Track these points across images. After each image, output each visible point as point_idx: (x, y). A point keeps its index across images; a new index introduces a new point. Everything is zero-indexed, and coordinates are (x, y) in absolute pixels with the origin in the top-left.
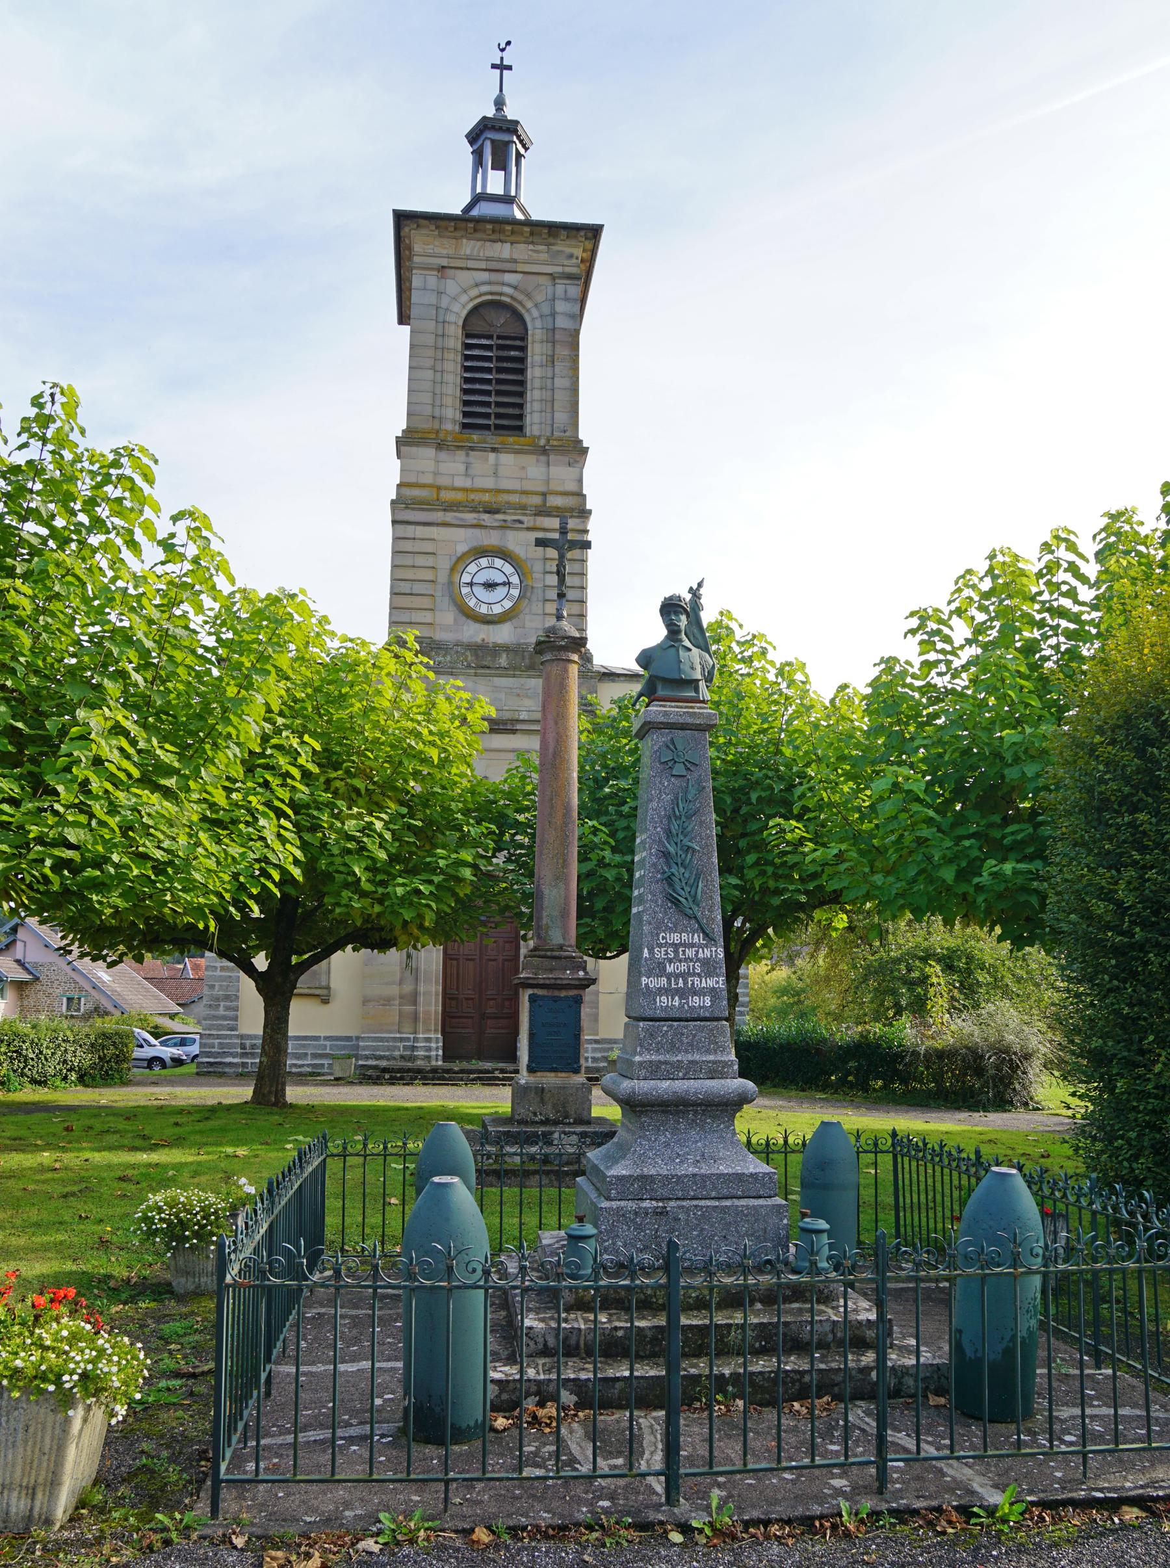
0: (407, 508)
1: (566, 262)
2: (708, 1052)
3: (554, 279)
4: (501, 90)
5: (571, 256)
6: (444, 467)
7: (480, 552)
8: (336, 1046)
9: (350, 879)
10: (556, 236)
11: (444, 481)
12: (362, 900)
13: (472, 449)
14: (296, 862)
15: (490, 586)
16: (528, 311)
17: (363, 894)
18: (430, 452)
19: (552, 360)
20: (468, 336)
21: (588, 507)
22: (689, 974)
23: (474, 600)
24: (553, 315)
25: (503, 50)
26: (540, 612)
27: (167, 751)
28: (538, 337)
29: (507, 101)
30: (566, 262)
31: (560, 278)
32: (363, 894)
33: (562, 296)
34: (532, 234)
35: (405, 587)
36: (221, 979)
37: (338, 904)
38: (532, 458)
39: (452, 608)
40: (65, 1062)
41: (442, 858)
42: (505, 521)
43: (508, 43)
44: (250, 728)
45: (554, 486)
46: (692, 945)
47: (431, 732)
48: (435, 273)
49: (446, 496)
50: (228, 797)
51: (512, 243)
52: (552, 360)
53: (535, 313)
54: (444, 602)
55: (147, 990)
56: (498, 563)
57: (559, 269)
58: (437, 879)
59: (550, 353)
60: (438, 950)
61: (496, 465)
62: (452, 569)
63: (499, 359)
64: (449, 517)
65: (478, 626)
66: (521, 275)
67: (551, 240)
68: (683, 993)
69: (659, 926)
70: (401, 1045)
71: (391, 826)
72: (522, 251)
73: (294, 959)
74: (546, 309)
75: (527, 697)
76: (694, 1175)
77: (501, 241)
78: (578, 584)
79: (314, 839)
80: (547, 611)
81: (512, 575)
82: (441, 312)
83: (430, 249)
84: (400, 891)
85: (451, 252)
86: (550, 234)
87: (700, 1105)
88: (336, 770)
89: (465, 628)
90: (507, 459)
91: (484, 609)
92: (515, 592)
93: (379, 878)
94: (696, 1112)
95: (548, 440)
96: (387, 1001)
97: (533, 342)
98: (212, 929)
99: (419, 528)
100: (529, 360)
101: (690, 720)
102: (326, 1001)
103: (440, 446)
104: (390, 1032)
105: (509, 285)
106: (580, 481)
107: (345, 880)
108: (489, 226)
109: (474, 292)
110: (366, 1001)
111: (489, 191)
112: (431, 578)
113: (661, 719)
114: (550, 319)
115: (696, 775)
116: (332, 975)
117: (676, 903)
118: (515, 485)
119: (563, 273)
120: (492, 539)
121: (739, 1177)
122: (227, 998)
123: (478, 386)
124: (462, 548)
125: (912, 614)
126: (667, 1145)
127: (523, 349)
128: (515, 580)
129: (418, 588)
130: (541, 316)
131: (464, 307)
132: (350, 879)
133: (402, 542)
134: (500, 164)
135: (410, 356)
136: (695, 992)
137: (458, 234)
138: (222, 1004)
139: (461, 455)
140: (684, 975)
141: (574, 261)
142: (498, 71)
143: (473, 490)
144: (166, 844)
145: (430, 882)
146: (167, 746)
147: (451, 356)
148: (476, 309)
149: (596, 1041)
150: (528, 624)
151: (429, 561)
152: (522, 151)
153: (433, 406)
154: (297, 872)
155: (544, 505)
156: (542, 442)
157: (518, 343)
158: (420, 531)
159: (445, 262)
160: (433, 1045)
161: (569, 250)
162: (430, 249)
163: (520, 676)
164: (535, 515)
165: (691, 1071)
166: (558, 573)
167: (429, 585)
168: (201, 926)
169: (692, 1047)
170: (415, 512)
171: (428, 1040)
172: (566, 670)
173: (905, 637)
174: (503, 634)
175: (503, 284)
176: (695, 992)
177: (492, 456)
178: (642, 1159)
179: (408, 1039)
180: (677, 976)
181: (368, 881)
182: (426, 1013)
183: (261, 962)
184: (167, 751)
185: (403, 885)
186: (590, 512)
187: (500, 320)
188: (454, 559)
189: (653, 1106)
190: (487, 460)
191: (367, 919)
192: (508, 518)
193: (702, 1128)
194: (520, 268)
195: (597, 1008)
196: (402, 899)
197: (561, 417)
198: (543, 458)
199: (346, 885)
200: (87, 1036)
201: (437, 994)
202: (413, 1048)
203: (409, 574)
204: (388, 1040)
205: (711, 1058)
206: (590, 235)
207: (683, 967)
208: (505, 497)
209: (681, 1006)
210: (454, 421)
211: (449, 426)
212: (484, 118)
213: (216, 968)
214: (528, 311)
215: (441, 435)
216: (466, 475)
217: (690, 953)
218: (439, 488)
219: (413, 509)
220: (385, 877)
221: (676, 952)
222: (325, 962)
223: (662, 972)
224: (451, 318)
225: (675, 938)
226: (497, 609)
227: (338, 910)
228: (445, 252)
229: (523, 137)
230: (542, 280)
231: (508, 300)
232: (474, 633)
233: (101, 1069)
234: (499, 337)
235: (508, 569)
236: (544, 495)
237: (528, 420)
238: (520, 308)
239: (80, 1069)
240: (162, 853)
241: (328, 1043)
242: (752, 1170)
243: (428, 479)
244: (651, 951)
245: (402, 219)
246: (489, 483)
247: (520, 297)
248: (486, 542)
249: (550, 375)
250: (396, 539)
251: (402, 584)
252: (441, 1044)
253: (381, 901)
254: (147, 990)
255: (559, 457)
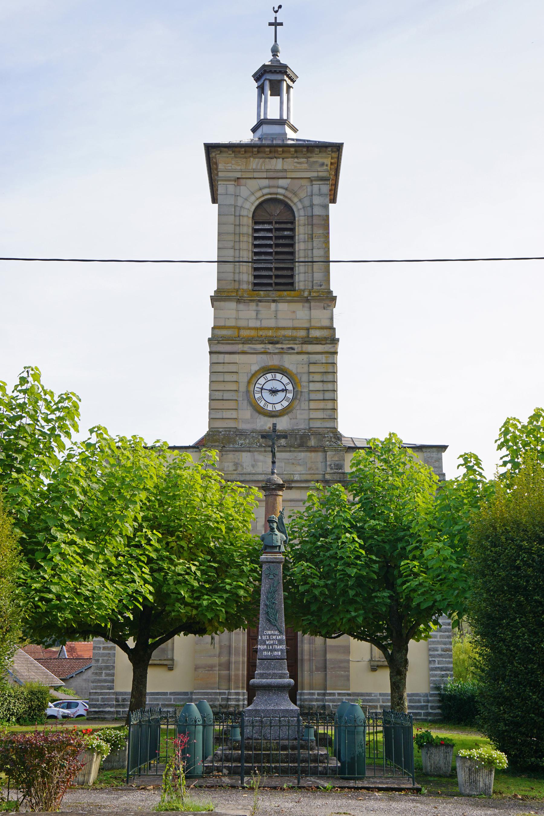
0: (218, 343)
1: (319, 169)
2: (279, 670)
3: (312, 181)
4: (276, 41)
5: (323, 164)
6: (242, 315)
7: (266, 370)
8: (178, 698)
9: (179, 596)
10: (312, 152)
11: (242, 323)
12: (186, 608)
13: (260, 301)
14: (151, 593)
15: (274, 392)
16: (295, 204)
17: (186, 604)
18: (233, 305)
19: (311, 237)
20: (256, 223)
21: (337, 337)
22: (274, 644)
23: (263, 402)
24: (312, 206)
25: (276, 12)
26: (307, 408)
27: (91, 544)
28: (302, 222)
29: (280, 48)
30: (319, 169)
31: (315, 180)
32: (186, 604)
33: (317, 192)
34: (296, 152)
35: (218, 395)
36: (103, 655)
37: (174, 611)
38: (300, 305)
39: (249, 408)
40: (9, 709)
41: (228, 584)
42: (282, 348)
43: (280, 7)
44: (128, 528)
45: (314, 323)
46: (275, 635)
47: (221, 517)
48: (233, 183)
49: (244, 333)
50: (117, 560)
51: (283, 159)
52: (311, 237)
53: (300, 206)
54: (244, 404)
55: (37, 668)
56: (279, 376)
57: (315, 174)
58: (225, 596)
59: (310, 232)
60: (243, 634)
61: (276, 311)
62: (249, 382)
63: (277, 238)
64: (246, 347)
65: (266, 419)
66: (290, 180)
67: (309, 155)
68: (271, 651)
69: (265, 629)
70: (219, 697)
71: (202, 567)
72: (289, 164)
73: (150, 641)
74: (307, 203)
75: (300, 465)
76: (273, 709)
77: (276, 158)
78: (331, 388)
79: (159, 576)
80: (311, 408)
81: (288, 384)
82: (238, 209)
83: (229, 167)
84: (205, 603)
85: (243, 167)
86: (308, 151)
87: (276, 687)
88: (172, 537)
89: (258, 420)
90: (283, 306)
91: (270, 408)
92: (290, 396)
93: (195, 595)
94: (275, 690)
95: (310, 292)
96: (211, 667)
97: (299, 226)
98: (109, 627)
99: (227, 356)
100: (297, 237)
101: (275, 560)
102: (171, 669)
103: (239, 301)
104: (213, 689)
105: (282, 188)
106: (332, 319)
107: (177, 597)
108: (268, 150)
109: (259, 194)
110: (197, 668)
111: (269, 117)
112: (235, 388)
113: (265, 560)
114: (309, 209)
115: (277, 578)
116: (175, 651)
117: (270, 621)
118: (289, 324)
119: (318, 177)
120: (275, 361)
121: (287, 711)
122: (107, 668)
123: (263, 257)
124: (255, 368)
125: (461, 456)
126: (266, 700)
127: (293, 230)
128: (290, 387)
129: (227, 396)
130: (304, 207)
131: (252, 204)
132: (179, 596)
133: (216, 365)
134: (276, 91)
135: (218, 241)
136: (275, 650)
137: (247, 155)
138: (104, 672)
139: (253, 306)
140: (272, 645)
141: (325, 167)
142: (274, 27)
143: (261, 329)
144: (90, 587)
145: (221, 597)
146: (91, 542)
147: (245, 239)
148: (261, 204)
149: (349, 695)
150: (299, 416)
151: (234, 377)
152: (290, 83)
153: (234, 273)
154: (150, 598)
155: (308, 337)
156: (306, 294)
157: (289, 226)
158: (228, 358)
159: (239, 175)
160: (241, 697)
161: (321, 160)
162: (229, 167)
163: (294, 451)
164: (302, 344)
165: (274, 676)
166: (272, 452)
167: (233, 393)
168: (103, 625)
169: (274, 668)
170: (224, 346)
171: (237, 694)
172: (276, 500)
173: (458, 467)
174: (283, 424)
175: (278, 187)
176: (275, 650)
177: (273, 305)
178: (257, 704)
179: (224, 693)
180: (270, 645)
181: (189, 597)
182: (237, 676)
183: (131, 643)
184: (91, 544)
185: (208, 599)
186: (338, 340)
187: (276, 211)
188: (250, 375)
189: (261, 687)
190: (270, 308)
191: (189, 618)
192: (285, 346)
193: (278, 695)
194: (289, 175)
195: (349, 671)
196: (207, 607)
197: (318, 276)
198: (307, 305)
199: (178, 600)
200: (22, 693)
201: (243, 662)
202: (228, 699)
203: (221, 387)
204: (210, 694)
205: (280, 672)
206: (335, 149)
207: (272, 642)
208: (283, 332)
209: (271, 655)
210: (248, 283)
211: (245, 286)
212: (264, 66)
213: (100, 648)
214: (295, 204)
215: (240, 293)
216: (257, 319)
217: (274, 637)
218: (239, 328)
219: (222, 344)
220: (198, 594)
221: (269, 637)
222: (170, 641)
223: (265, 644)
224: (244, 213)
225: (269, 632)
226: (279, 407)
227: (173, 614)
228: (239, 168)
229: (291, 75)
230: (304, 182)
231: (281, 197)
232: (265, 424)
233: (29, 715)
234: (276, 223)
235: (285, 380)
236: (308, 329)
237: (297, 278)
238: (289, 202)
239: (17, 714)
240: (89, 592)
241: (172, 697)
242: (291, 708)
243: (232, 323)
244: (261, 637)
245: (210, 148)
246: (272, 323)
247: (289, 195)
248: (270, 363)
249: (310, 247)
250: (212, 364)
251: (217, 393)
252: (246, 697)
253: (196, 608)
254: (37, 668)
255: (317, 304)
